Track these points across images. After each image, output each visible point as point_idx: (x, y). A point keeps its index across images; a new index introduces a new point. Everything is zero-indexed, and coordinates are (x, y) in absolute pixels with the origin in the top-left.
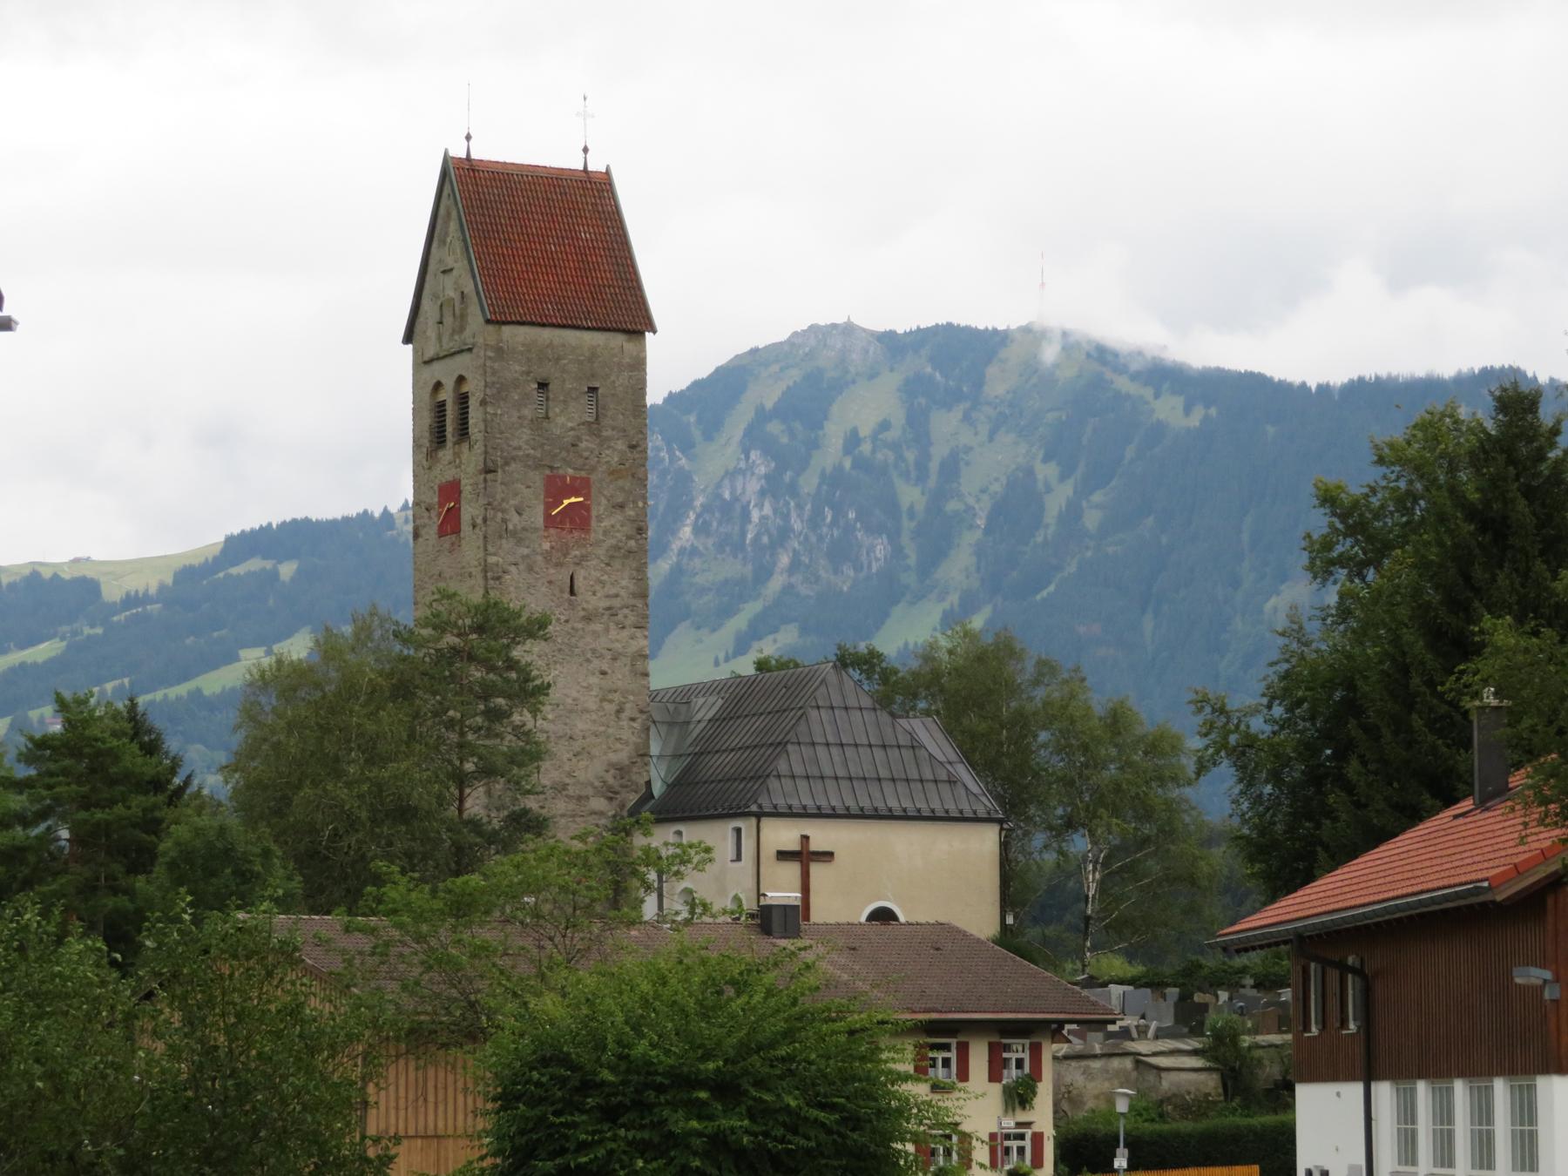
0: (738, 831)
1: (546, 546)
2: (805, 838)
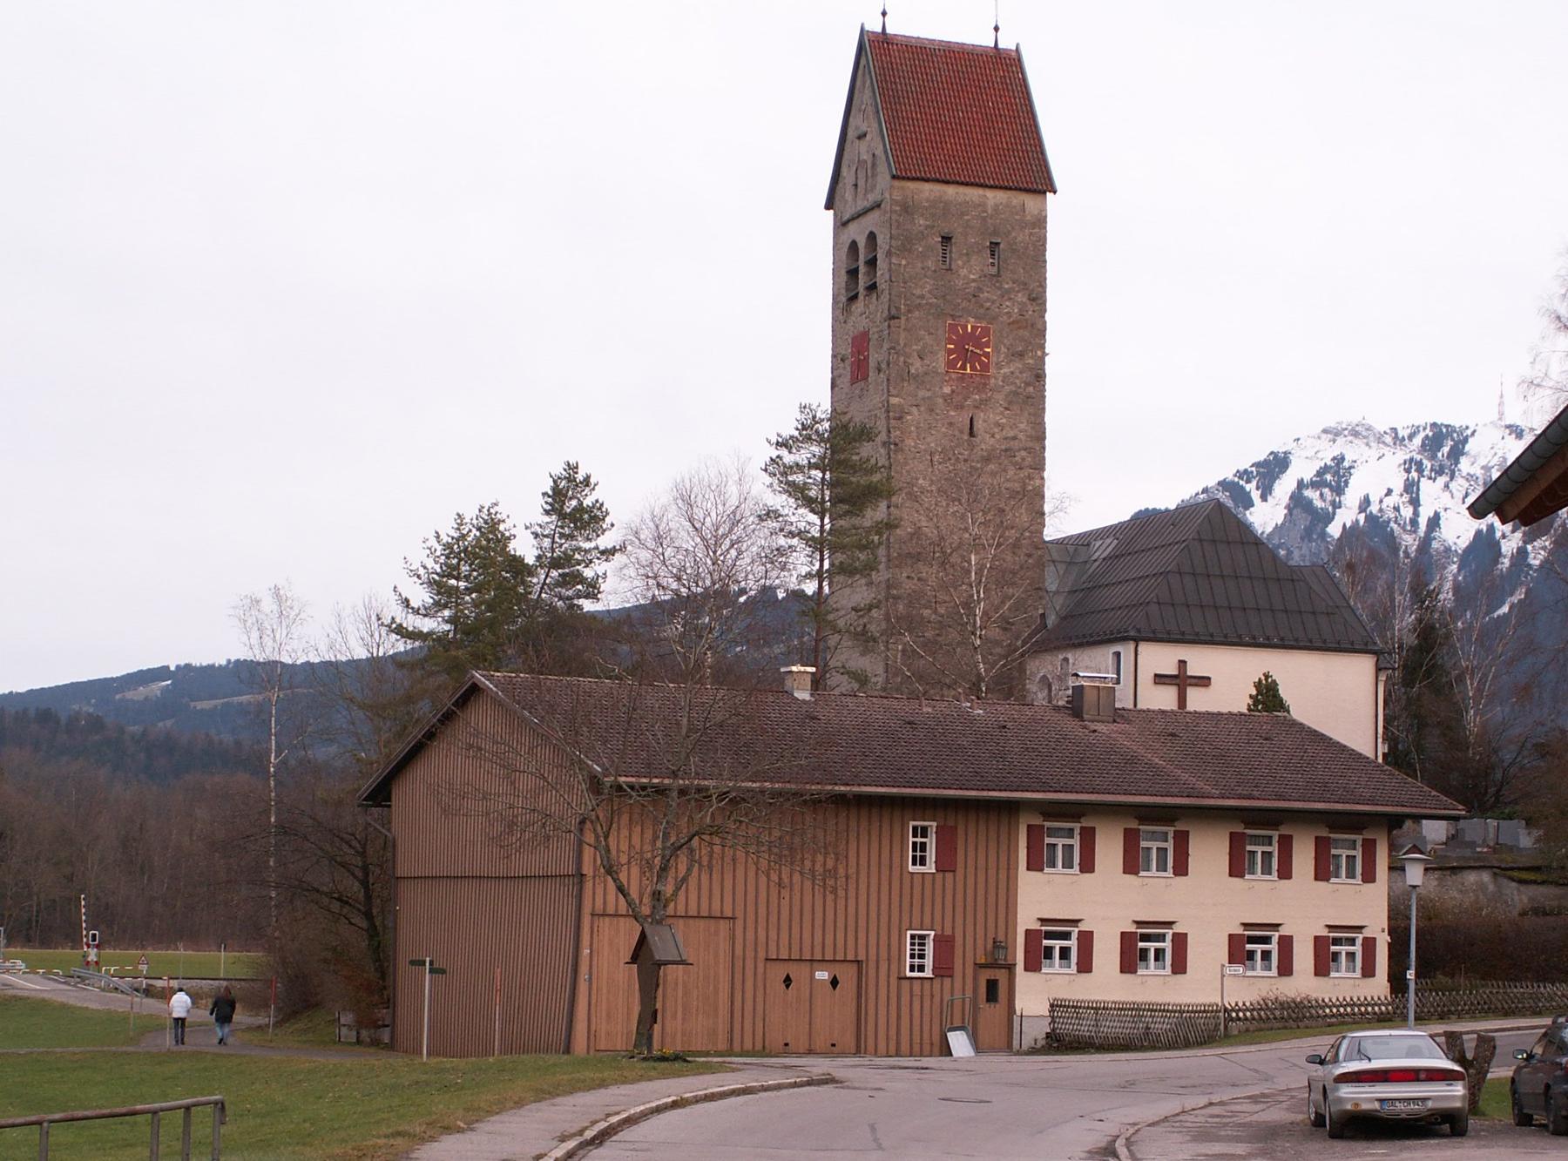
0: (1118, 655)
1: (947, 390)
2: (1182, 663)
